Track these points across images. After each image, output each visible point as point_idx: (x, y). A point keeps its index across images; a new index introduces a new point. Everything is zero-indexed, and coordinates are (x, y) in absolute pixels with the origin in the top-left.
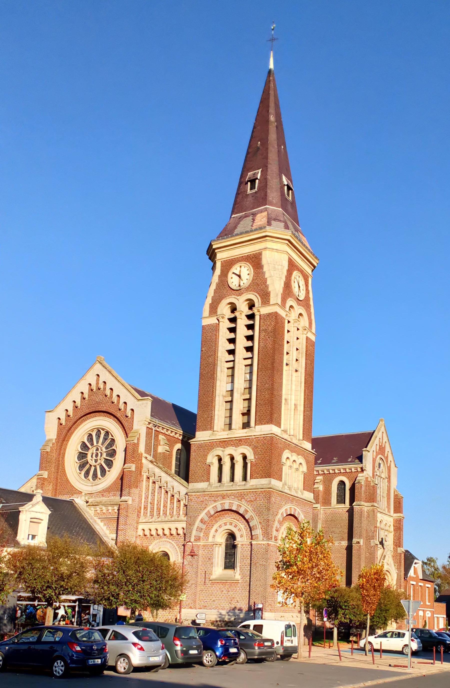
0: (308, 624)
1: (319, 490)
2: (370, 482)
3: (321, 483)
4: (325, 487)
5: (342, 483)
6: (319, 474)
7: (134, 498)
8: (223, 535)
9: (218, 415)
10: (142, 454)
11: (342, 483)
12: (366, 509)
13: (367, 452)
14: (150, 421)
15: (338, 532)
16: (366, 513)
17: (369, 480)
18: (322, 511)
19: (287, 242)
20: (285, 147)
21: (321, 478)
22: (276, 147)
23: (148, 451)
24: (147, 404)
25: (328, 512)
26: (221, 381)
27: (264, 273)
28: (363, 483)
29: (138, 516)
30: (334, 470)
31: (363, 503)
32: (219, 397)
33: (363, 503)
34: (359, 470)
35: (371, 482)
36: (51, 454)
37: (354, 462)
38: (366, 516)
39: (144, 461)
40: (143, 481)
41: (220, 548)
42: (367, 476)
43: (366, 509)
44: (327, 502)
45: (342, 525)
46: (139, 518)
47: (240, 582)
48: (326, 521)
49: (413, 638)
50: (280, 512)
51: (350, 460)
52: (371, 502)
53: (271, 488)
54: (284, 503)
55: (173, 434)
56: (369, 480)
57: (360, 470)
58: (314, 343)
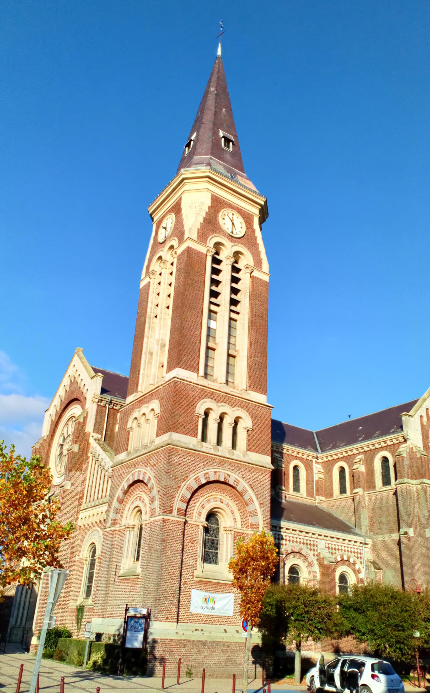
0: (263, 644)
1: (359, 471)
2: (416, 452)
3: (361, 462)
4: (368, 468)
5: (385, 460)
6: (359, 453)
7: (75, 482)
8: (136, 515)
9: (143, 374)
10: (90, 433)
11: (385, 460)
12: (414, 488)
13: (407, 417)
14: (100, 398)
15: (387, 522)
16: (416, 494)
17: (414, 450)
18: (366, 497)
19: (207, 179)
20: (229, 110)
21: (361, 456)
22: (213, 109)
23: (97, 429)
24: (98, 382)
25: (374, 497)
26: (148, 338)
27: (182, 215)
28: (405, 455)
29: (80, 503)
30: (373, 445)
31: (406, 480)
32: (145, 355)
33: (406, 480)
34: (402, 440)
35: (417, 453)
36: (40, 451)
37: (396, 431)
38: (415, 498)
39: (91, 440)
40: (88, 463)
41: (132, 532)
42: (411, 446)
43: (414, 488)
44: (371, 485)
45: (390, 512)
46: (81, 505)
47: (140, 577)
48: (372, 509)
49: (376, 673)
50: (192, 477)
51: (392, 430)
52: (420, 479)
53: (169, 444)
54: (202, 465)
55: (325, 460)
56: (414, 450)
57: (403, 440)
58: (268, 283)
